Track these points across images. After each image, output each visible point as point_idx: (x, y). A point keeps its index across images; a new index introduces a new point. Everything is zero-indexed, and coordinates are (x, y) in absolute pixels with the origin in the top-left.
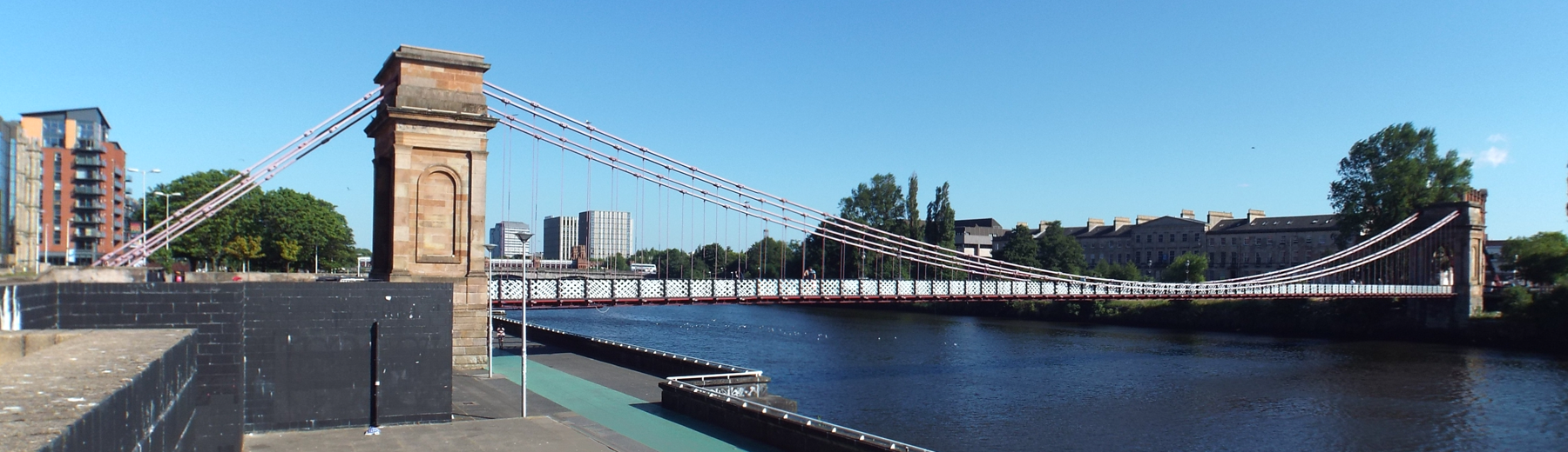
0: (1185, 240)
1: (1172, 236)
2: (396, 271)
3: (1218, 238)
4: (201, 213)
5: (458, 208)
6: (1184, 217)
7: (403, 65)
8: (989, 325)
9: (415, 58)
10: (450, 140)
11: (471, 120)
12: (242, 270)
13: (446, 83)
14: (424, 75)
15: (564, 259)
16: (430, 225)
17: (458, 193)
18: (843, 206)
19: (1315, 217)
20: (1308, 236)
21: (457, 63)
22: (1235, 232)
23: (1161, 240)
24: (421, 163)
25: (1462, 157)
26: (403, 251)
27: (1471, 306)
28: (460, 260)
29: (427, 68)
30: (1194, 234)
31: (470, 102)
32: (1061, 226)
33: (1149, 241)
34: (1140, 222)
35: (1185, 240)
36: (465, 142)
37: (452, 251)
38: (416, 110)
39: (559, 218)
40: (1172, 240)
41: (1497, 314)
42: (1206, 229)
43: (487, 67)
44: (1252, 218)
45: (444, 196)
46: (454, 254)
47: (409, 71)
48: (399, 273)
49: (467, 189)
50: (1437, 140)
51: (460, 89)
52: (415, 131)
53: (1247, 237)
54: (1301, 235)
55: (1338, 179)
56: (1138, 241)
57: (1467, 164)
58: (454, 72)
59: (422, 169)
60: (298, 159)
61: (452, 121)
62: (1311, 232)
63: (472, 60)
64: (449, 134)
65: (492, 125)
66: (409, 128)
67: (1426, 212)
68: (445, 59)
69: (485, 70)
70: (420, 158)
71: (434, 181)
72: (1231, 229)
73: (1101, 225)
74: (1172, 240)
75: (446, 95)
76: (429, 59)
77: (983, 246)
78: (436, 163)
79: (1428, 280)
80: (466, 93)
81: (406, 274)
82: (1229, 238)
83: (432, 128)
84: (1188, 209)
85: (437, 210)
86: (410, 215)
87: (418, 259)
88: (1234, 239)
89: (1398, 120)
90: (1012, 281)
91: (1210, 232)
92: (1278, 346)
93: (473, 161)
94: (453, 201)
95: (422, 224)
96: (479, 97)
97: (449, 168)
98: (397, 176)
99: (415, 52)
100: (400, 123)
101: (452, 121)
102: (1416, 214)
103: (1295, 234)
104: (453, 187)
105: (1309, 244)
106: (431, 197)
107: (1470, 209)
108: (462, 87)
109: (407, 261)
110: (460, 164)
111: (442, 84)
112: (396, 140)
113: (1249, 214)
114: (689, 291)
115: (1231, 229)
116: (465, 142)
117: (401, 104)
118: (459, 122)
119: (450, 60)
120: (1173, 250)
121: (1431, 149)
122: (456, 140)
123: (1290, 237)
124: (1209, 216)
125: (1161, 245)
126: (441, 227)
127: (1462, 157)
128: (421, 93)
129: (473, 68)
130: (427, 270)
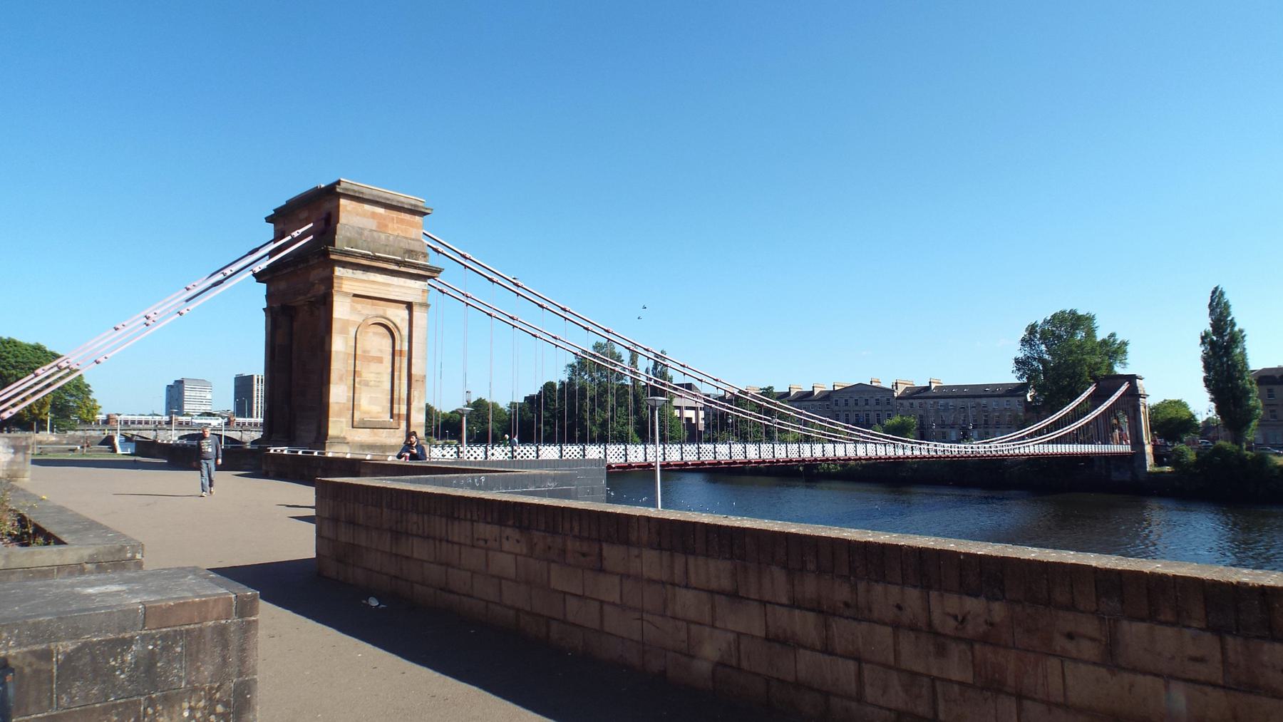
0: (878, 404)
1: (867, 400)
2: (332, 438)
3: (906, 403)
4: (56, 369)
5: (397, 365)
6: (874, 384)
7: (343, 202)
8: (993, 498)
9: (357, 195)
10: (391, 289)
11: (415, 268)
12: (46, 430)
13: (386, 226)
14: (364, 215)
15: (257, 417)
16: (367, 384)
17: (397, 348)
18: (569, 372)
19: (987, 386)
20: (984, 401)
21: (400, 205)
22: (921, 398)
23: (856, 404)
24: (359, 313)
25: (1119, 338)
26: (339, 414)
27: (1147, 462)
28: (399, 425)
29: (367, 207)
30: (885, 399)
31: (411, 248)
32: (774, 391)
33: (847, 405)
34: (836, 388)
35: (878, 404)
36: (406, 291)
37: (389, 415)
38: (360, 253)
39: (252, 376)
40: (867, 404)
41: (1167, 469)
42: (896, 395)
44: (933, 386)
45: (381, 351)
46: (392, 417)
47: (349, 209)
48: (336, 440)
49: (407, 344)
50: (1097, 322)
51: (401, 234)
52: (355, 276)
53: (931, 402)
54: (978, 400)
55: (1020, 355)
56: (837, 405)
57: (1125, 344)
58: (394, 214)
59: (359, 319)
60: (187, 301)
61: (396, 268)
62: (986, 399)
63: (413, 202)
64: (390, 282)
65: (435, 275)
67: (1101, 383)
68: (388, 199)
69: (426, 214)
70: (359, 307)
71: (371, 334)
72: (917, 395)
73: (800, 390)
74: (867, 404)
75: (387, 238)
76: (371, 198)
77: (688, 408)
78: (374, 313)
79: (1109, 440)
80: (406, 238)
81: (342, 441)
82: (916, 402)
83: (372, 274)
84: (875, 378)
85: (374, 367)
86: (347, 371)
87: (355, 423)
88: (921, 404)
90: (875, 444)
91: (899, 398)
92: (986, 500)
93: (415, 313)
94: (391, 357)
95: (360, 383)
96: (420, 243)
97: (389, 320)
98: (336, 326)
99: (356, 188)
100: (339, 266)
101: (396, 268)
102: (1095, 384)
103: (972, 399)
104: (390, 341)
105: (986, 409)
106: (368, 352)
107: (1138, 380)
108: (402, 231)
109: (344, 425)
110: (398, 316)
111: (382, 227)
112: (335, 285)
113: (930, 382)
114: (537, 453)
115: (917, 395)
116: (406, 291)
117: (340, 243)
118: (403, 269)
119: (392, 200)
120: (867, 412)
121: (1091, 333)
122: (397, 290)
123: (970, 402)
125: (857, 408)
126: (378, 386)
127: (1119, 338)
128: (361, 234)
129: (414, 211)
130: (364, 436)
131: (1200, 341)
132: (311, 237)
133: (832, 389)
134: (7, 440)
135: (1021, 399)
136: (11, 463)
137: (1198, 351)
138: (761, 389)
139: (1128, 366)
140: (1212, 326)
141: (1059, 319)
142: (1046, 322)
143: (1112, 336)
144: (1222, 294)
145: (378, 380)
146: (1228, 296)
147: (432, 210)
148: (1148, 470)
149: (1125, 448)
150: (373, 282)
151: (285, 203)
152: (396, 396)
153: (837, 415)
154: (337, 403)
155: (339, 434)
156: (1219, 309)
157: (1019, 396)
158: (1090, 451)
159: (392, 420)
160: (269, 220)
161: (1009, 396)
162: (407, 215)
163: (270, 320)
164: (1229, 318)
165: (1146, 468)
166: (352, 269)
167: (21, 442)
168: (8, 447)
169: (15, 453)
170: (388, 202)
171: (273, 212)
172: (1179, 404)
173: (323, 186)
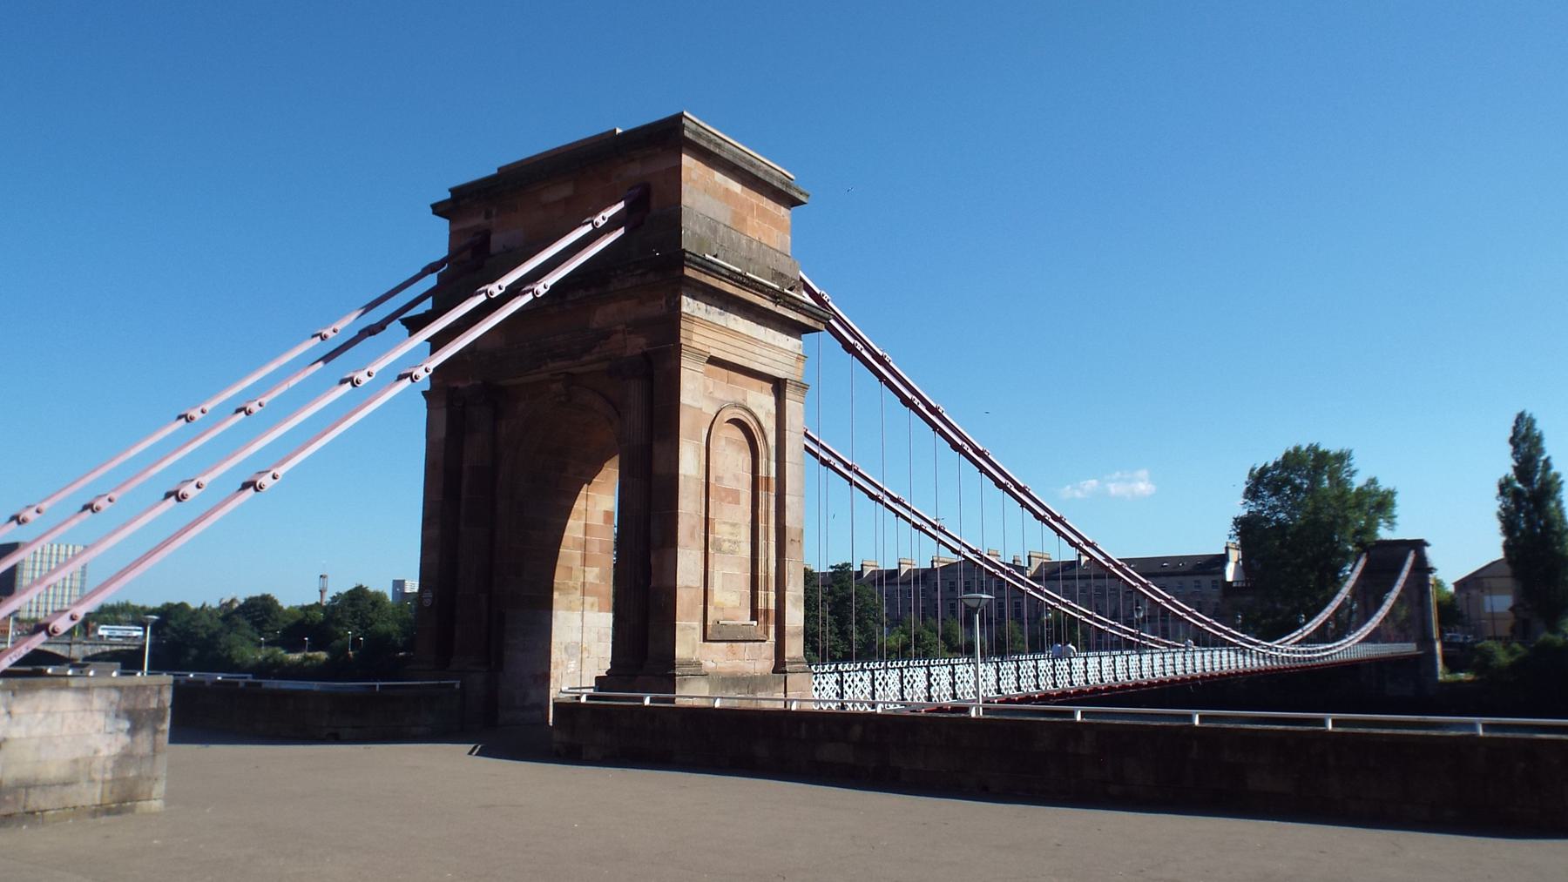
9: (704, 143)
13: (744, 220)
29: (718, 177)
43: (802, 198)
46: (754, 616)
47: (694, 176)
55: (1244, 513)
57: (1392, 493)
61: (769, 305)
62: (1164, 578)
66: (714, 314)
89: (1304, 441)
97: (752, 414)
124: (1029, 557)
128: (715, 231)
131: (1497, 491)
132: (621, 231)
133: (930, 567)
134: (115, 695)
135: (1217, 578)
136: (125, 758)
137: (1491, 505)
138: (832, 567)
139: (1396, 527)
140: (1515, 468)
141: (1292, 461)
142: (1276, 464)
143: (1372, 484)
144: (1531, 422)
145: (734, 538)
146: (1539, 426)
147: (808, 196)
148: (1440, 678)
149: (1410, 648)
150: (725, 330)
151: (495, 171)
152: (761, 574)
153: (1089, 599)
154: (687, 587)
155: (690, 656)
156: (1525, 441)
157: (1213, 573)
158: (1225, 653)
159: (755, 623)
160: (439, 209)
161: (1198, 574)
162: (770, 201)
163: (442, 415)
164: (1543, 458)
165: (1436, 675)
166: (706, 303)
167: (148, 700)
168: (117, 716)
169: (133, 731)
170: (753, 170)
171: (448, 196)
172: (385, 594)
173: (619, 131)
